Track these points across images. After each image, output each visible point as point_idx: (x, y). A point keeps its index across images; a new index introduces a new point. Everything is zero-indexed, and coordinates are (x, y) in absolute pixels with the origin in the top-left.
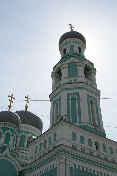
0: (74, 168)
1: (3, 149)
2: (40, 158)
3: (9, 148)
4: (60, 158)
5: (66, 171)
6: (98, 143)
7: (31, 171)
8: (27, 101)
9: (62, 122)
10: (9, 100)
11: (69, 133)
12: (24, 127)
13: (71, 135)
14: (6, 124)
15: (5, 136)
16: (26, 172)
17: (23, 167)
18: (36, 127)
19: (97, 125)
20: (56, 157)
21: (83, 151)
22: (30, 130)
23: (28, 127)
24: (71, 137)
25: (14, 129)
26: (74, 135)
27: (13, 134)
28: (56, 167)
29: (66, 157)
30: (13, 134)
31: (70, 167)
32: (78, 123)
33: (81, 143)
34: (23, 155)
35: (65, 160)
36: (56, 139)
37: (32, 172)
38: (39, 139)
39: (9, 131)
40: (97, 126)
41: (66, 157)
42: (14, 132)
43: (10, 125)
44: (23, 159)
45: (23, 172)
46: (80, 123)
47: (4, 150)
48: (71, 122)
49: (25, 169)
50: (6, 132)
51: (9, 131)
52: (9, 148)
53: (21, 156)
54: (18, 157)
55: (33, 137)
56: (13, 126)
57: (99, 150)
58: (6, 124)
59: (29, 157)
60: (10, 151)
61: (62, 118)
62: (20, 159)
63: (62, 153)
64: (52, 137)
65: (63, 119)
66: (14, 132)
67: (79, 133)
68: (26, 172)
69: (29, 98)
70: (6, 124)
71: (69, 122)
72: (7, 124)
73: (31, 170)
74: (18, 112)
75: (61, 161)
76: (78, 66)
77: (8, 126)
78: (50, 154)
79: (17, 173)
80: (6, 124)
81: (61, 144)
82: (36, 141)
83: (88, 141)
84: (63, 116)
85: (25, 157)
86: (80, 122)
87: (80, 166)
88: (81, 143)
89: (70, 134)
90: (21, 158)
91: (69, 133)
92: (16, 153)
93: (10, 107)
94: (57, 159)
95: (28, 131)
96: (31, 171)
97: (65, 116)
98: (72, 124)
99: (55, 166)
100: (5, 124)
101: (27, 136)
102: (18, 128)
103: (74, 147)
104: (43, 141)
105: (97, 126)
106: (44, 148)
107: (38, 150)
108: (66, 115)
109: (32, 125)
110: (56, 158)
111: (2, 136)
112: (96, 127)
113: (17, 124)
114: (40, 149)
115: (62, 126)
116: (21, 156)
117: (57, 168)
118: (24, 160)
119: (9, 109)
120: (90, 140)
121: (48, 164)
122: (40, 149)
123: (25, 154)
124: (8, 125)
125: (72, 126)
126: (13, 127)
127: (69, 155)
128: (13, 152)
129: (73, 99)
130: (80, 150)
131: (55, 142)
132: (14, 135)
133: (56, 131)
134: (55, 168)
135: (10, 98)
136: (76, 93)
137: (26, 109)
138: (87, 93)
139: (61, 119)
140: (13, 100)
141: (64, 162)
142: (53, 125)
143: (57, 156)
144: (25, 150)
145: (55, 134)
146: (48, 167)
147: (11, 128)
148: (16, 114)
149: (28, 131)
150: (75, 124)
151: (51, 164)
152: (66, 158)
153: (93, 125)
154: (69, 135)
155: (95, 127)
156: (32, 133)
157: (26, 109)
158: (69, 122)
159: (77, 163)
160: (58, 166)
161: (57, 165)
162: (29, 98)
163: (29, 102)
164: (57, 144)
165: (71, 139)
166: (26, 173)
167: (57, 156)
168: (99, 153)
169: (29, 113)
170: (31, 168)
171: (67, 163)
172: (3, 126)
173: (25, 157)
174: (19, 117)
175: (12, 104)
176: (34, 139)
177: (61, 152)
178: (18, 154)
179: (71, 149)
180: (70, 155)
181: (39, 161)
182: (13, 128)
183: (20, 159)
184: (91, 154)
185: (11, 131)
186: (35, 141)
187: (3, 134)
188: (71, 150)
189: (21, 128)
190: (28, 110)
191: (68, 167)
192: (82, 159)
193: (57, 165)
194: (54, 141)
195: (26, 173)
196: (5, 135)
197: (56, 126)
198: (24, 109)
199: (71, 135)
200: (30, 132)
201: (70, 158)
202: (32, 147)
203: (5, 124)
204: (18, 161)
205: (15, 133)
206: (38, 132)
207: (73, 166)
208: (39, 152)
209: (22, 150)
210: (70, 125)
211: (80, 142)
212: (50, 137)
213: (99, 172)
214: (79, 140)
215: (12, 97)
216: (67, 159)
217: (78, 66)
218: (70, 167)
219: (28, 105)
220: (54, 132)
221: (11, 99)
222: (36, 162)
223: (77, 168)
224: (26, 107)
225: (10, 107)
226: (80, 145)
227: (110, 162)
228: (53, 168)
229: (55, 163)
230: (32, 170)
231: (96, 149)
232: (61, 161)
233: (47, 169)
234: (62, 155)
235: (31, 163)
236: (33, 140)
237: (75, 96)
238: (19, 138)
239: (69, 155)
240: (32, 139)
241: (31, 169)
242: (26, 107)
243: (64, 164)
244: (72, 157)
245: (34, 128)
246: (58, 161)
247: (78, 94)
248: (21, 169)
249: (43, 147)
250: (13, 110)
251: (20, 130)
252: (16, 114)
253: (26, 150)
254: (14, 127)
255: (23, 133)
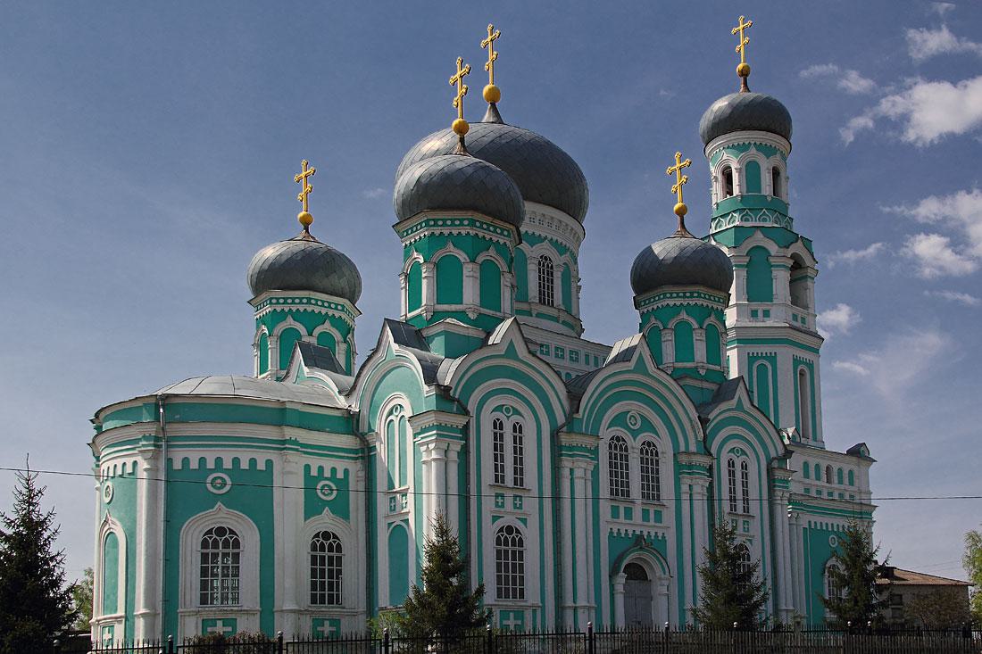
19: (714, 451)
39: (492, 252)
51: (492, 252)
76: (777, 266)
85: (557, 348)
95: (537, 233)
129: (762, 368)
136: (769, 355)
138: (796, 313)
144: (534, 314)
149: (537, 233)
173: (557, 348)
185: (499, 252)
192: (393, 450)
204: (551, 367)
217: (777, 266)
237: (765, 362)
243: (583, 481)
245: (554, 216)
247: (772, 359)
253: (538, 315)
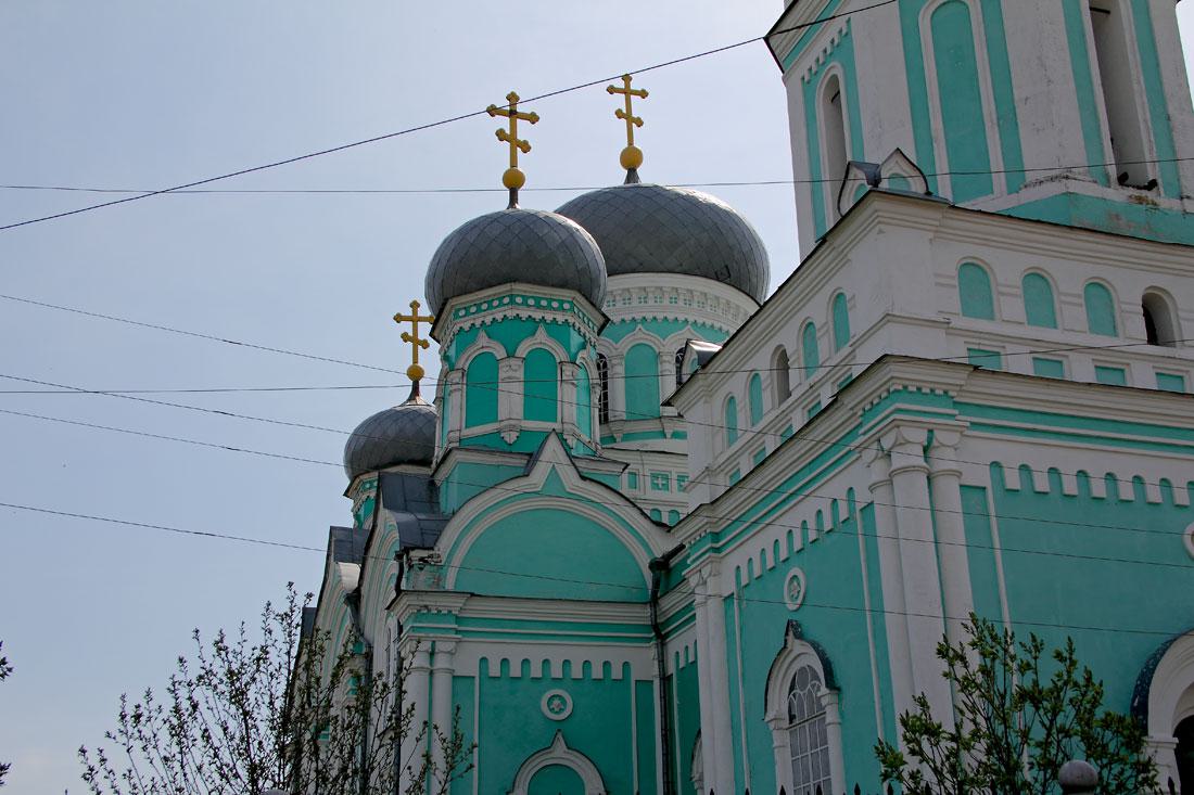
0: (990, 492)
1: (530, 455)
2: (762, 463)
3: (563, 441)
4: (887, 443)
5: (939, 515)
6: (1165, 297)
7: (718, 550)
8: (625, 115)
9: (876, 204)
10: (501, 135)
11: (937, 275)
12: (627, 294)
13: (1016, 296)
14: (512, 302)
15: (520, 374)
16: (691, 559)
17: (669, 531)
18: (718, 279)
20: (861, 439)
21: (1111, 383)
22: (681, 303)
23: (661, 288)
24: (952, 301)
25: (571, 320)
26: (974, 276)
27: (573, 350)
28: (872, 503)
29: (931, 431)
30: (573, 350)
31: (961, 486)
32: (999, 181)
33: (1035, 324)
34: (659, 464)
35: (925, 450)
36: (852, 332)
37: (724, 553)
38: (738, 347)
39: (541, 335)
40: (1152, 185)
41: (931, 431)
42: (576, 340)
43: (537, 300)
44: (666, 487)
45: (673, 562)
46: (1013, 189)
47: (532, 458)
48: (944, 190)
49: (682, 547)
50: (522, 351)
51: (541, 335)
52: (563, 441)
53: (654, 476)
54: (634, 485)
55: (696, 348)
56: (562, 302)
57: (1170, 343)
58: (512, 297)
59: (693, 468)
60: (573, 453)
61: (875, 181)
62: (651, 494)
63: (898, 410)
64: (817, 326)
65: (884, 185)
66: (576, 340)
67: (1008, 265)
68: (691, 559)
69: (636, 93)
70: (512, 297)
71: (928, 198)
72: (519, 300)
73: (717, 542)
74: (582, 208)
75: (898, 461)
77: (564, 310)
78: (823, 428)
79: (640, 570)
80: (512, 302)
81: (886, 355)
82: (724, 365)
83: (1082, 301)
84: (878, 166)
86: (1016, 174)
87: (1063, 477)
88: (1095, 327)
89: (942, 281)
90: (655, 486)
91: (937, 275)
92: (615, 462)
93: (513, 182)
94: (869, 455)
96: (718, 550)
97: (898, 158)
98: (953, 207)
99: (862, 497)
100: (506, 300)
101: (672, 345)
102: (599, 310)
103: (976, 362)
104: (763, 361)
105: (1152, 185)
106: (781, 402)
107: (960, 518)
108: (898, 149)
109: (685, 273)
110: (862, 448)
111: (502, 375)
112: (1144, 193)
113: (586, 288)
114: (756, 412)
115: (881, 232)
116: (654, 476)
117: (876, 508)
118: (674, 495)
119: (513, 199)
120: (1097, 287)
121: (817, 493)
122: (756, 412)
123: (674, 459)
124: (525, 303)
125: (950, 222)
126: (563, 306)
127: (952, 416)
128: (595, 457)
130: (1027, 368)
131: (846, 350)
132: (580, 355)
133: (841, 281)
134: (861, 510)
135: (504, 123)
137: (632, 174)
139: (869, 187)
140: (524, 130)
141: (921, 462)
142: (821, 245)
143: (864, 434)
144: (669, 433)
145: (839, 297)
146: (820, 512)
147: (549, 317)
148: (561, 218)
150: (981, 199)
151: (836, 488)
152: (930, 440)
153: (1123, 180)
154: (937, 284)
155: (1136, 193)
156: (700, 321)
157: (632, 174)
158: (928, 198)
159: (1013, 453)
160: (880, 496)
161: (872, 489)
162: (636, 93)
163: (640, 123)
164: (867, 356)
165: (957, 308)
166: (689, 566)
167: (864, 434)
168: (1170, 367)
169: (655, 192)
170: (717, 530)
171: (938, 466)
172: (499, 317)
174: (587, 236)
175: (524, 163)
176: (706, 360)
177: (892, 408)
178: (628, 465)
179: (960, 377)
180: (956, 412)
181: (756, 482)
182: (560, 318)
183: (648, 493)
184: (1111, 383)
186: (715, 366)
187: (506, 362)
188: (963, 382)
189: (619, 305)
190: (646, 176)
191: (950, 492)
193: (872, 489)
194: (838, 350)
195: (689, 562)
196: (522, 370)
197: (839, 241)
198: (618, 178)
199: (1016, 296)
200: (681, 318)
201: (958, 434)
202: (703, 412)
203: (506, 300)
205: (583, 347)
206: (738, 307)
207: (983, 477)
208: (749, 436)
209: (647, 441)
210: (939, 216)
211: (1023, 318)
212: (811, 323)
213: (1152, 479)
214: (1012, 307)
215: (513, 114)
216: (935, 443)
218: (961, 486)
219: (637, 145)
220: (828, 290)
221: (513, 127)
222: (741, 495)
223: (1013, 480)
224: (631, 160)
225: (513, 182)
226: (1021, 340)
227: (1090, 384)
228: (851, 511)
229: (859, 476)
230: (721, 543)
231: (1153, 338)
232: (898, 461)
233: (812, 524)
234: (896, 424)
235: (707, 501)
236: (704, 367)
238: (618, 370)
239: (952, 416)
240: (690, 359)
241: (716, 536)
242: (631, 160)
244: (972, 423)
246: (880, 466)
248: (662, 545)
249: (768, 398)
250: (542, 199)
251: (615, 318)
252: (561, 218)
254: (566, 306)
255: (641, 335)
